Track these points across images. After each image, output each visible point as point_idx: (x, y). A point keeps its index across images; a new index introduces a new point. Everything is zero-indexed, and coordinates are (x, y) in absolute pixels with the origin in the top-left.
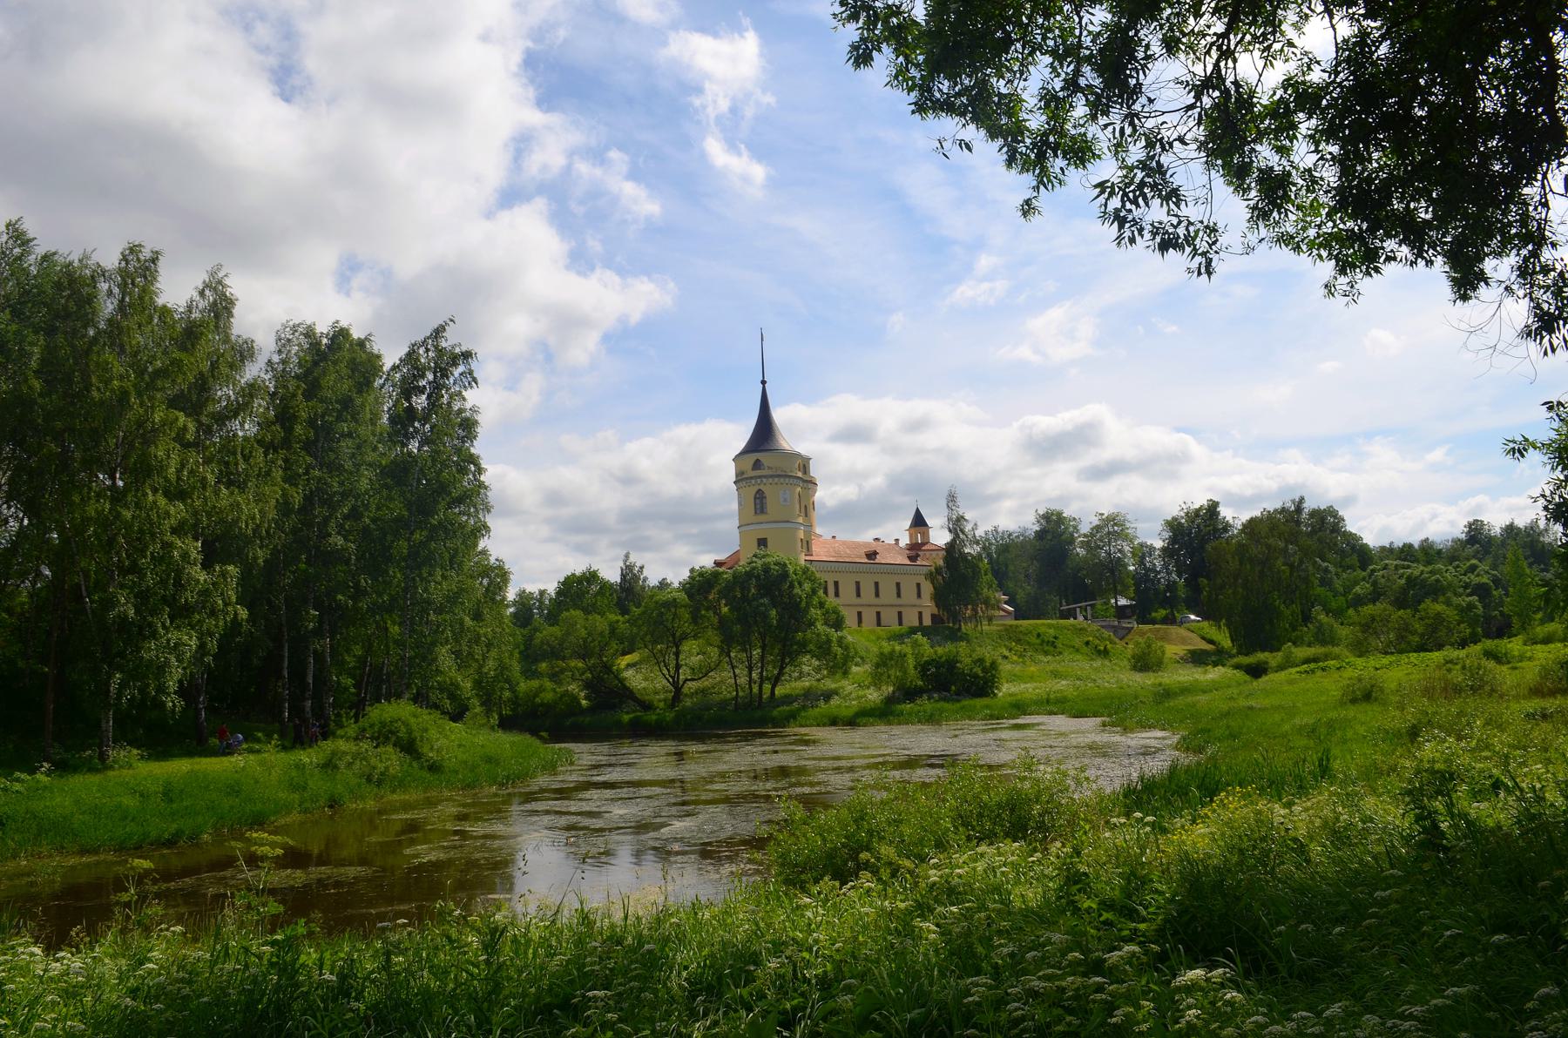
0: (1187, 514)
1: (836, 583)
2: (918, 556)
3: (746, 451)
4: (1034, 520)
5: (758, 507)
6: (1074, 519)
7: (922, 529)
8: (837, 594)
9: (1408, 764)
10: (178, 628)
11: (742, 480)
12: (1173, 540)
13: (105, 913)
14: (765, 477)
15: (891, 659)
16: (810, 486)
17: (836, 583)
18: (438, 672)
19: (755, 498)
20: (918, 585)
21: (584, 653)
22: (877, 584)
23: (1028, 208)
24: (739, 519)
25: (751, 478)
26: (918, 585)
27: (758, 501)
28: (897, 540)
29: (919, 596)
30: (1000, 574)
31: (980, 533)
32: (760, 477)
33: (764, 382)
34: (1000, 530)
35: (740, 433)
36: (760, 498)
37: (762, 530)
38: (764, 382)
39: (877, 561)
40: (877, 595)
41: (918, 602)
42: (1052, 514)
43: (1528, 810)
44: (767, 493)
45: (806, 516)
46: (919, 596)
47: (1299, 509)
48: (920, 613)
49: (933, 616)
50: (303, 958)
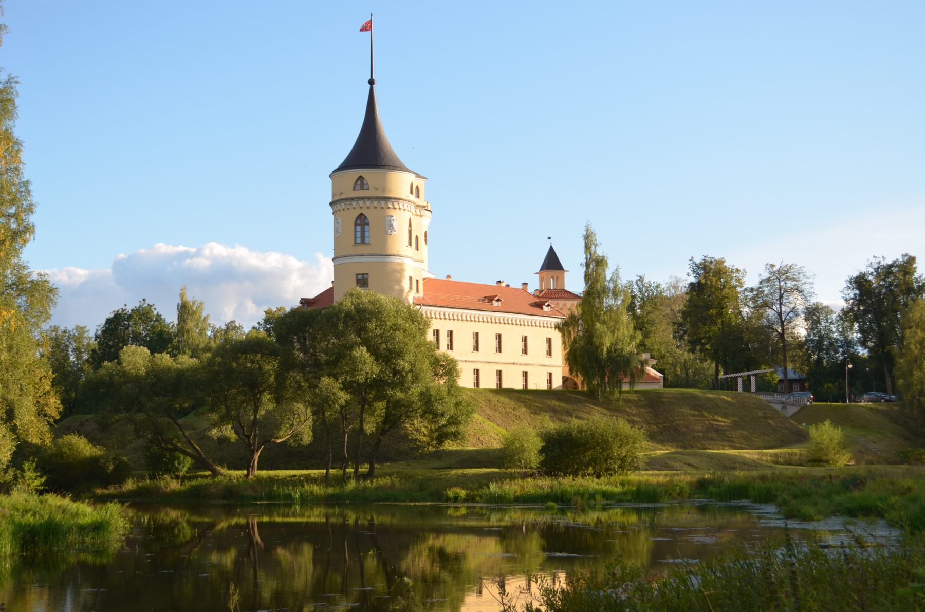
0: (877, 270)
1: (451, 334)
3: (348, 164)
5: (359, 234)
6: (738, 270)
9: (371, 396)
11: (340, 201)
12: (859, 300)
13: (797, 344)
14: (369, 198)
17: (451, 334)
19: (356, 224)
21: (634, 439)
22: (499, 337)
24: (335, 250)
25: (352, 199)
26: (549, 341)
27: (359, 228)
31: (623, 281)
32: (363, 198)
33: (371, 82)
34: (646, 280)
36: (362, 221)
38: (371, 82)
41: (548, 361)
42: (711, 262)
43: (413, 403)
45: (417, 249)
49: (565, 380)
50: (744, 314)
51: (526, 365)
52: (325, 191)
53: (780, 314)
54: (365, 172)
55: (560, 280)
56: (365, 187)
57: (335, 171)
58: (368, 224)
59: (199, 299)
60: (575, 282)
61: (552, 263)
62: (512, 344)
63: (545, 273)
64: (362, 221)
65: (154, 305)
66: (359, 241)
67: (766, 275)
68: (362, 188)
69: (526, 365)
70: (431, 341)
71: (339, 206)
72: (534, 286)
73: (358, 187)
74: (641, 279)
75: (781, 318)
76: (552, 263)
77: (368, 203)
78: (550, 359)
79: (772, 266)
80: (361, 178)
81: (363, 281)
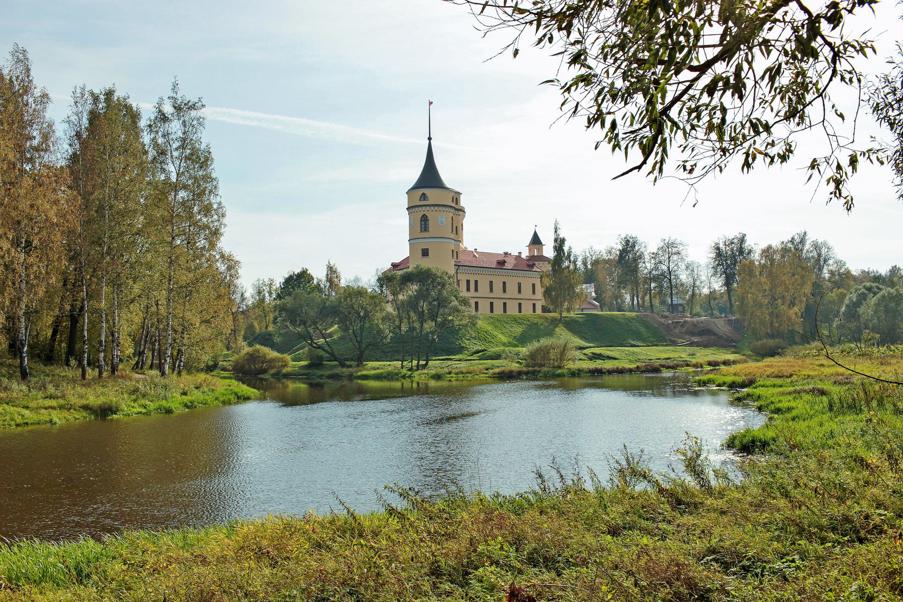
1: (476, 282)
2: (534, 265)
3: (417, 186)
4: (618, 241)
5: (423, 226)
7: (537, 246)
8: (476, 290)
10: (102, 263)
11: (412, 207)
15: (446, 393)
16: (460, 213)
17: (476, 282)
18: (95, 384)
19: (421, 221)
20: (534, 285)
22: (504, 283)
23: (175, 86)
26: (534, 285)
27: (423, 223)
28: (520, 253)
29: (534, 292)
30: (590, 277)
33: (430, 139)
34: (593, 249)
35: (415, 173)
36: (424, 219)
37: (424, 244)
38: (430, 139)
39: (504, 267)
40: (504, 291)
44: (429, 217)
46: (534, 292)
47: (803, 241)
48: (534, 305)
51: (520, 299)
52: (404, 202)
53: (669, 268)
54: (426, 191)
55: (540, 250)
56: (426, 199)
57: (409, 190)
58: (428, 220)
59: (587, 247)
60: (549, 252)
61: (536, 241)
62: (498, 287)
63: (531, 246)
64: (424, 219)
65: (688, 245)
66: (423, 229)
67: (661, 244)
68: (425, 200)
69: (520, 299)
70: (713, 293)
71: (411, 210)
72: (525, 254)
73: (422, 199)
74: (591, 248)
75: (669, 269)
76: (536, 241)
77: (428, 208)
78: (468, 293)
79: (665, 240)
80: (424, 194)
81: (425, 253)
